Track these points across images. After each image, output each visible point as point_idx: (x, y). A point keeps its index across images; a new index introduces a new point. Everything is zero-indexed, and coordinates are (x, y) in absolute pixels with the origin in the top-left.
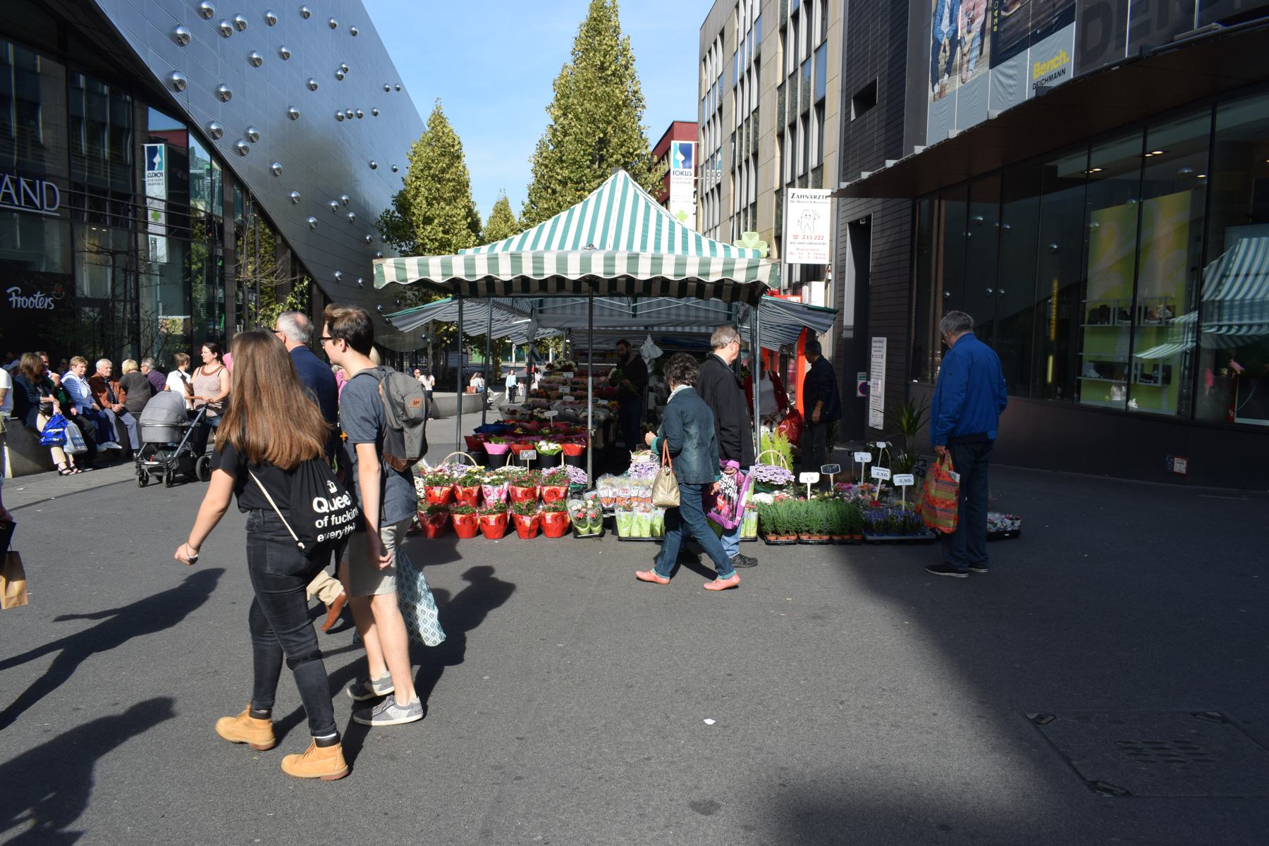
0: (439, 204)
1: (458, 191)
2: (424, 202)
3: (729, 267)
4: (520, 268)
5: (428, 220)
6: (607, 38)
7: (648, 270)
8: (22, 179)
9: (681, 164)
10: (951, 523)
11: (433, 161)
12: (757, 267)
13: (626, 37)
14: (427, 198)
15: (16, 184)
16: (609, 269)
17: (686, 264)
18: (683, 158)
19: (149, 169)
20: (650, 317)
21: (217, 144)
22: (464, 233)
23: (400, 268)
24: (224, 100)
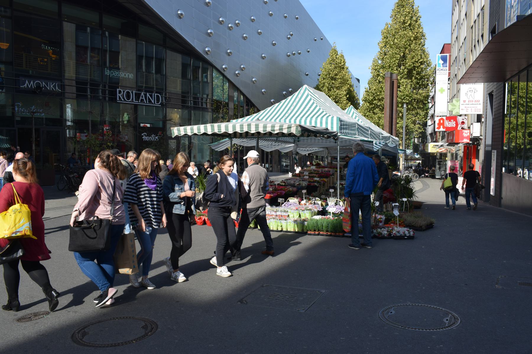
0: (334, 89)
1: (343, 83)
2: (327, 89)
3: (281, 128)
4: (214, 129)
6: (407, 9)
7: (254, 129)
8: (148, 93)
9: (441, 65)
10: (348, 228)
11: (331, 71)
12: (291, 127)
13: (417, 7)
14: (328, 87)
15: (146, 95)
16: (242, 129)
17: (266, 127)
18: (443, 62)
20: (342, 143)
21: (226, 73)
22: (345, 102)
23: (179, 130)
24: (229, 55)
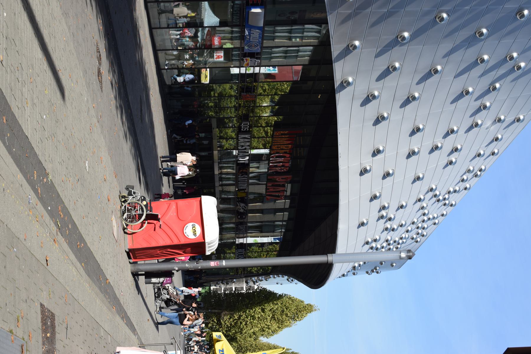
5: (263, 310)
19: (274, 239)
